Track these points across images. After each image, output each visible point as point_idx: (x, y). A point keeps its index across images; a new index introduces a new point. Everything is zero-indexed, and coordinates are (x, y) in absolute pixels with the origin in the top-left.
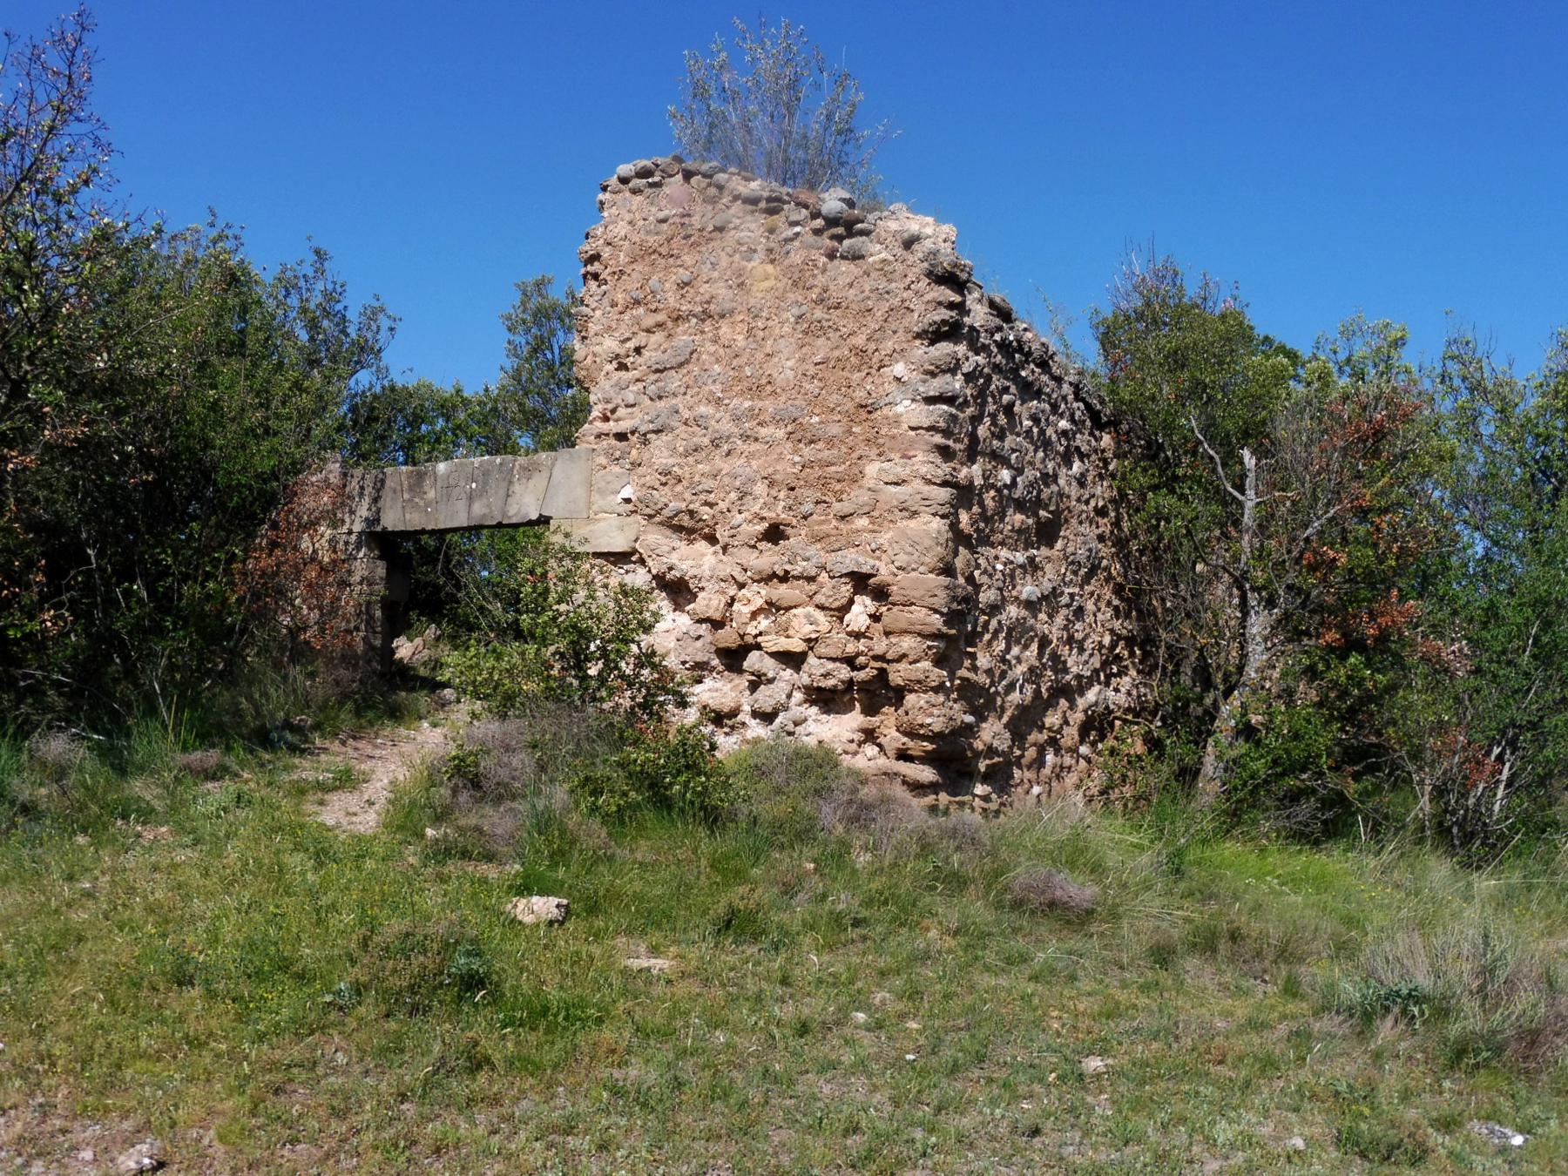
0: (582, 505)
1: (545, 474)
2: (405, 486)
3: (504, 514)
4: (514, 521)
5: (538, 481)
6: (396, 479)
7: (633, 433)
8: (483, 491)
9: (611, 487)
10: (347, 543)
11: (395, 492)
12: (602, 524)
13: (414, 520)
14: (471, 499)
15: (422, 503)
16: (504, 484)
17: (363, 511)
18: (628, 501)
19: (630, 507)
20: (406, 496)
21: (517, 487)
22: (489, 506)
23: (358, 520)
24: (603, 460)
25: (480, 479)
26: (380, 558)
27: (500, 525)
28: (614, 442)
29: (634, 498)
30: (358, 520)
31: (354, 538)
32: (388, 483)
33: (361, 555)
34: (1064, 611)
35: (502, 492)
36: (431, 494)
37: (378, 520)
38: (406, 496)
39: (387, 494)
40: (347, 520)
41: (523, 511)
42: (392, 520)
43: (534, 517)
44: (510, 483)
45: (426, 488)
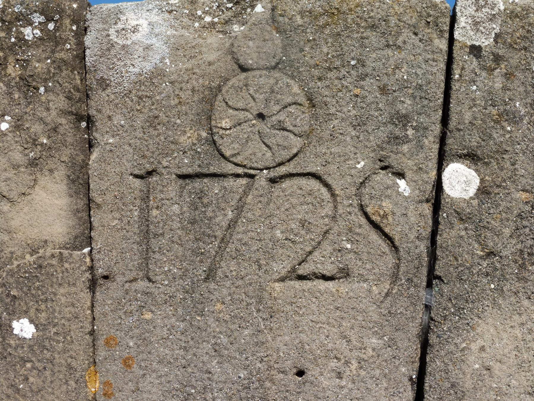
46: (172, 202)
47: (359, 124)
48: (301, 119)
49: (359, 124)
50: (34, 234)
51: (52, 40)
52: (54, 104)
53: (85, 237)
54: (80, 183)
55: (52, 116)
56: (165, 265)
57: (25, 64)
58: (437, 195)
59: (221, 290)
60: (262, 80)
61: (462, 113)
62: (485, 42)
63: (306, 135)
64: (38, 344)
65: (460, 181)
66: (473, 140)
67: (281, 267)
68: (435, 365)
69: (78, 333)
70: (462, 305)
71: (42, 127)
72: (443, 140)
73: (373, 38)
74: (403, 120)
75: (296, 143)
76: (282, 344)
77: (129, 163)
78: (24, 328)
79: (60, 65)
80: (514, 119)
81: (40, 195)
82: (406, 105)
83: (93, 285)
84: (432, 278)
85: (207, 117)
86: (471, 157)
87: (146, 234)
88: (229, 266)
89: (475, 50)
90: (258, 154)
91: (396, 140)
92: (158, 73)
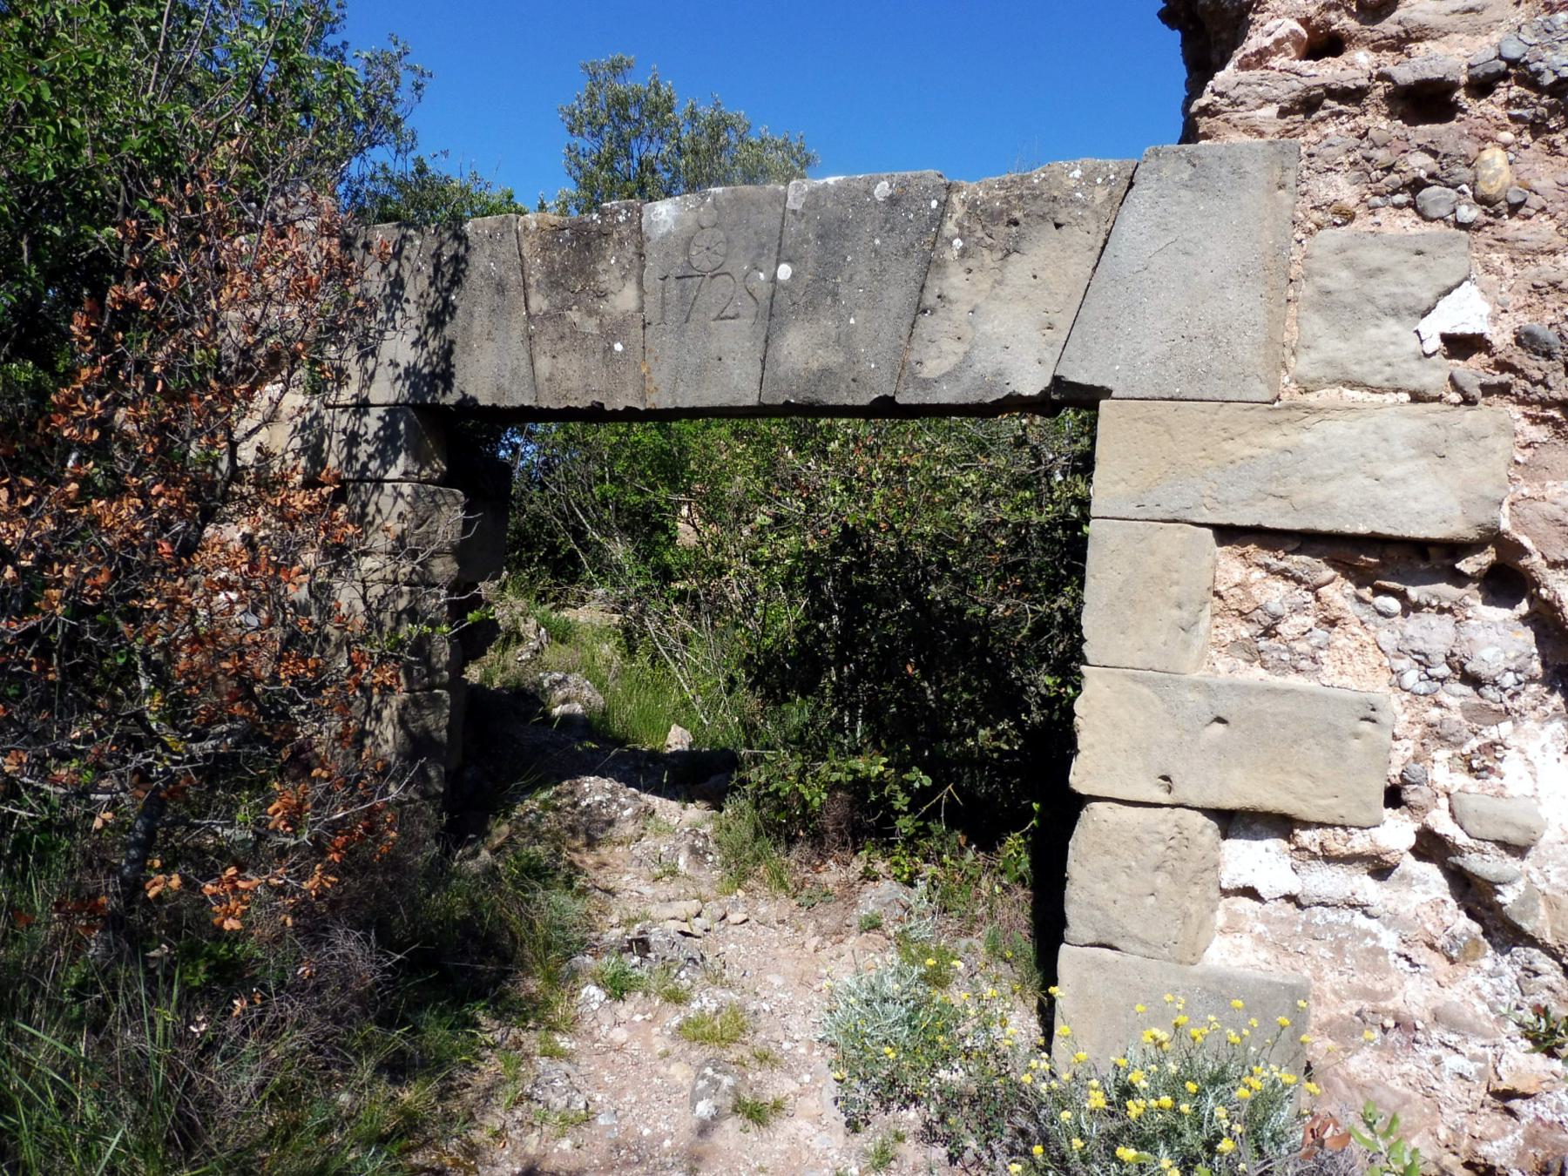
0: (1247, 352)
1: (1082, 238)
2: (535, 276)
3: (904, 370)
4: (945, 395)
5: (1054, 261)
6: (506, 250)
7: (1482, 86)
8: (821, 291)
9: (1382, 289)
10: (353, 439)
11: (501, 288)
12: (1337, 428)
13: (567, 378)
14: (773, 314)
15: (591, 326)
16: (912, 268)
17: (400, 348)
18: (1460, 345)
19: (1473, 370)
20: (538, 303)
21: (955, 281)
22: (844, 341)
23: (384, 376)
24: (1344, 189)
25: (812, 249)
26: (447, 481)
27: (885, 408)
28: (1379, 123)
29: (1501, 338)
30: (384, 376)
31: (372, 423)
32: (480, 263)
33: (394, 473)
34: (1226, 1123)
35: (897, 297)
36: (625, 299)
37: (446, 377)
38: (538, 303)
39: (474, 302)
40: (354, 370)
41: (984, 364)
42: (485, 376)
43: (1031, 383)
44: (931, 265)
45: (607, 280)
46: (673, 287)
47: (746, 249)
48: (722, 249)
49: (746, 249)
50: (623, 308)
51: (629, 221)
52: (631, 249)
53: (641, 309)
54: (640, 283)
55: (630, 255)
56: (671, 317)
57: (619, 233)
58: (774, 279)
59: (691, 326)
60: (708, 232)
61: (787, 241)
62: (798, 207)
63: (726, 256)
64: (624, 353)
65: (784, 272)
66: (791, 253)
67: (713, 315)
68: (770, 352)
69: (639, 347)
70: (781, 325)
71: (651, 863)
72: (779, 253)
73: (753, 209)
74: (762, 246)
75: (721, 259)
76: (713, 347)
77: (658, 273)
78: (618, 347)
79: (632, 231)
80: (807, 242)
81: (626, 290)
82: (765, 239)
83: (644, 327)
84: (771, 315)
85: (687, 251)
86: (789, 261)
87: (664, 303)
88: (693, 316)
89: (794, 212)
90: (707, 266)
91: (760, 255)
92: (669, 233)
